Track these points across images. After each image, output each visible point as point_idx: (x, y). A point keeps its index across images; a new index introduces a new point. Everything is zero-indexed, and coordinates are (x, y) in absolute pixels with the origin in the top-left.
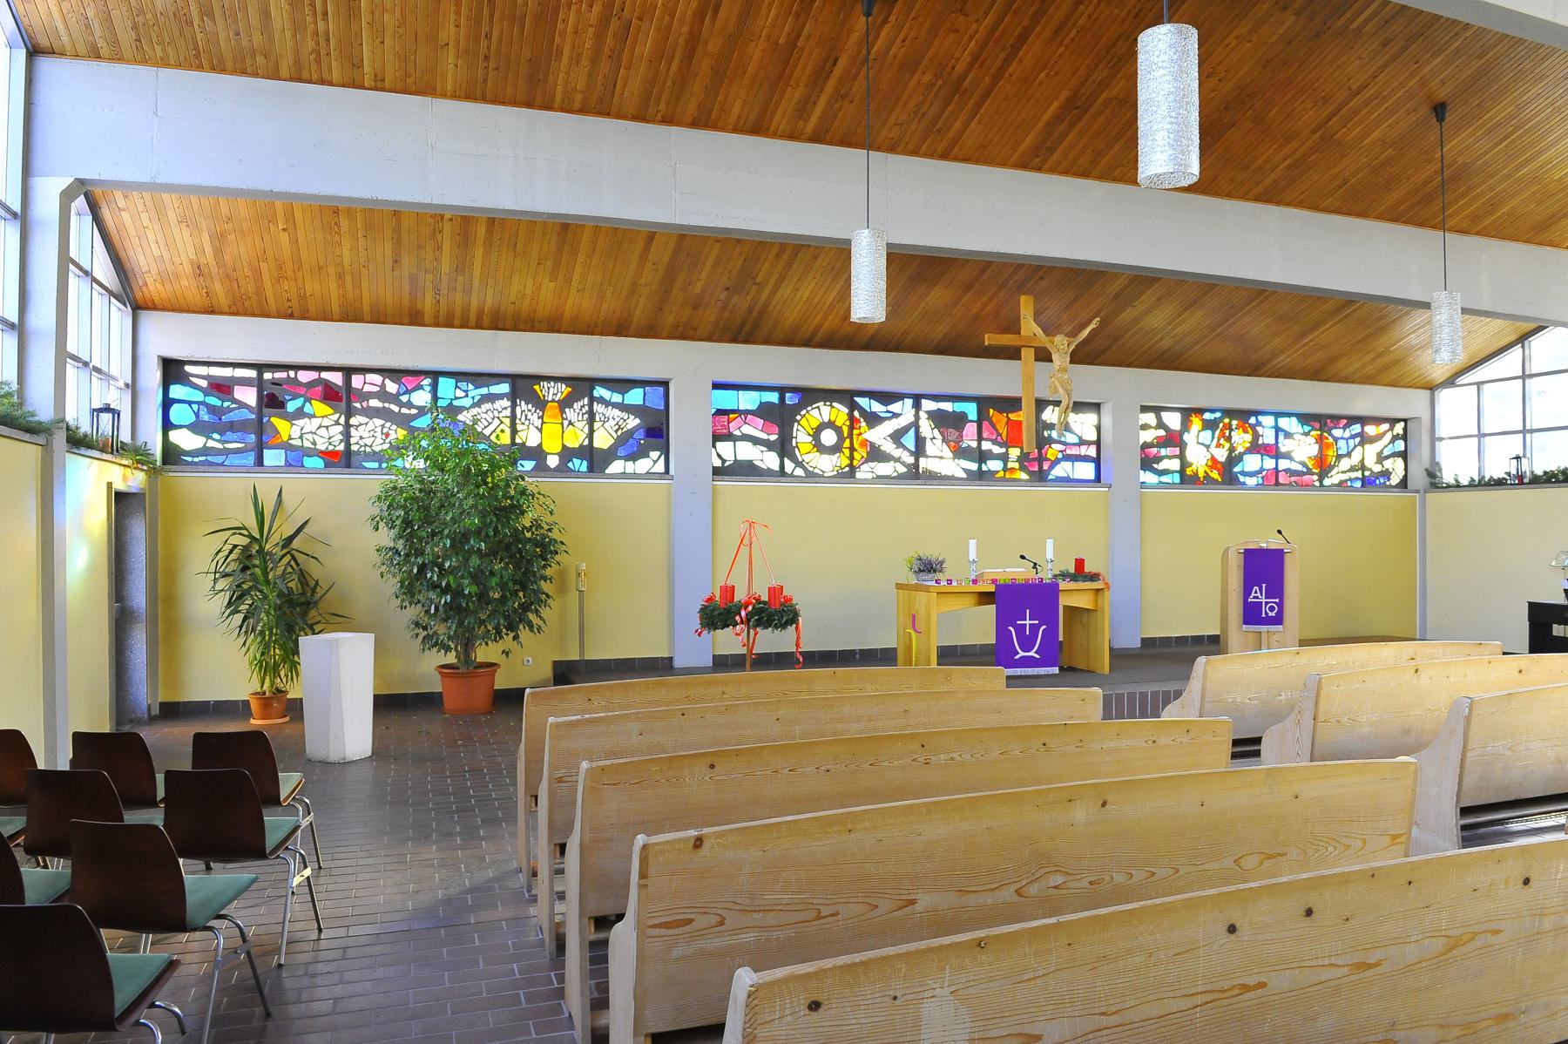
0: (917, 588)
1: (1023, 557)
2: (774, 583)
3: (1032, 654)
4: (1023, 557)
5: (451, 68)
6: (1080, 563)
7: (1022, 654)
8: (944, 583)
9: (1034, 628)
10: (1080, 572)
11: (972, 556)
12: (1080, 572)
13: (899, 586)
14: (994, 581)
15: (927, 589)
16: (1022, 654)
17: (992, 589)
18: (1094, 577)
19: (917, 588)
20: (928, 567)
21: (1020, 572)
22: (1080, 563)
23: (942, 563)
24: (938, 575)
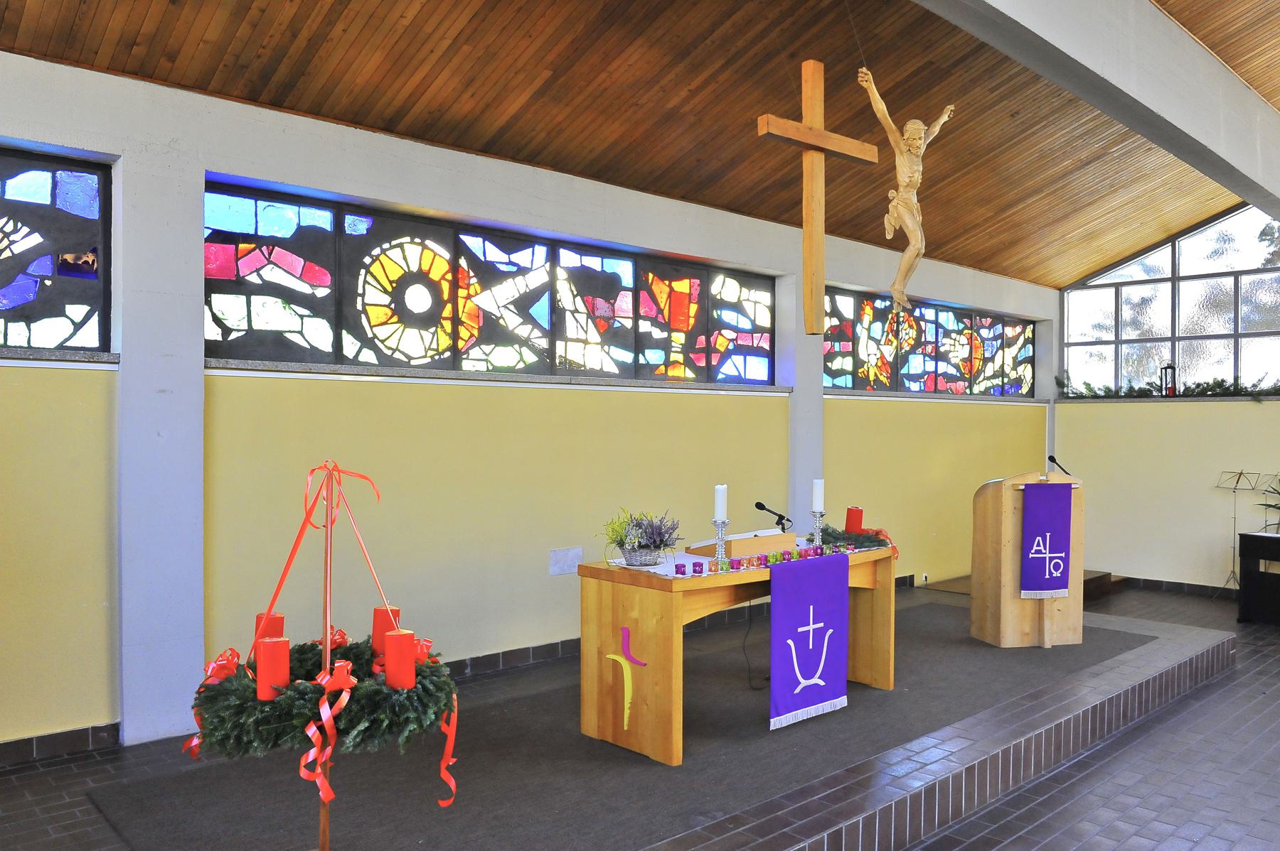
0: (633, 577)
1: (760, 506)
4: (760, 506)
6: (854, 516)
7: (804, 683)
9: (819, 634)
10: (857, 534)
13: (587, 572)
14: (763, 561)
15: (664, 585)
17: (763, 575)
18: (875, 539)
20: (656, 538)
22: (854, 516)
23: (674, 528)
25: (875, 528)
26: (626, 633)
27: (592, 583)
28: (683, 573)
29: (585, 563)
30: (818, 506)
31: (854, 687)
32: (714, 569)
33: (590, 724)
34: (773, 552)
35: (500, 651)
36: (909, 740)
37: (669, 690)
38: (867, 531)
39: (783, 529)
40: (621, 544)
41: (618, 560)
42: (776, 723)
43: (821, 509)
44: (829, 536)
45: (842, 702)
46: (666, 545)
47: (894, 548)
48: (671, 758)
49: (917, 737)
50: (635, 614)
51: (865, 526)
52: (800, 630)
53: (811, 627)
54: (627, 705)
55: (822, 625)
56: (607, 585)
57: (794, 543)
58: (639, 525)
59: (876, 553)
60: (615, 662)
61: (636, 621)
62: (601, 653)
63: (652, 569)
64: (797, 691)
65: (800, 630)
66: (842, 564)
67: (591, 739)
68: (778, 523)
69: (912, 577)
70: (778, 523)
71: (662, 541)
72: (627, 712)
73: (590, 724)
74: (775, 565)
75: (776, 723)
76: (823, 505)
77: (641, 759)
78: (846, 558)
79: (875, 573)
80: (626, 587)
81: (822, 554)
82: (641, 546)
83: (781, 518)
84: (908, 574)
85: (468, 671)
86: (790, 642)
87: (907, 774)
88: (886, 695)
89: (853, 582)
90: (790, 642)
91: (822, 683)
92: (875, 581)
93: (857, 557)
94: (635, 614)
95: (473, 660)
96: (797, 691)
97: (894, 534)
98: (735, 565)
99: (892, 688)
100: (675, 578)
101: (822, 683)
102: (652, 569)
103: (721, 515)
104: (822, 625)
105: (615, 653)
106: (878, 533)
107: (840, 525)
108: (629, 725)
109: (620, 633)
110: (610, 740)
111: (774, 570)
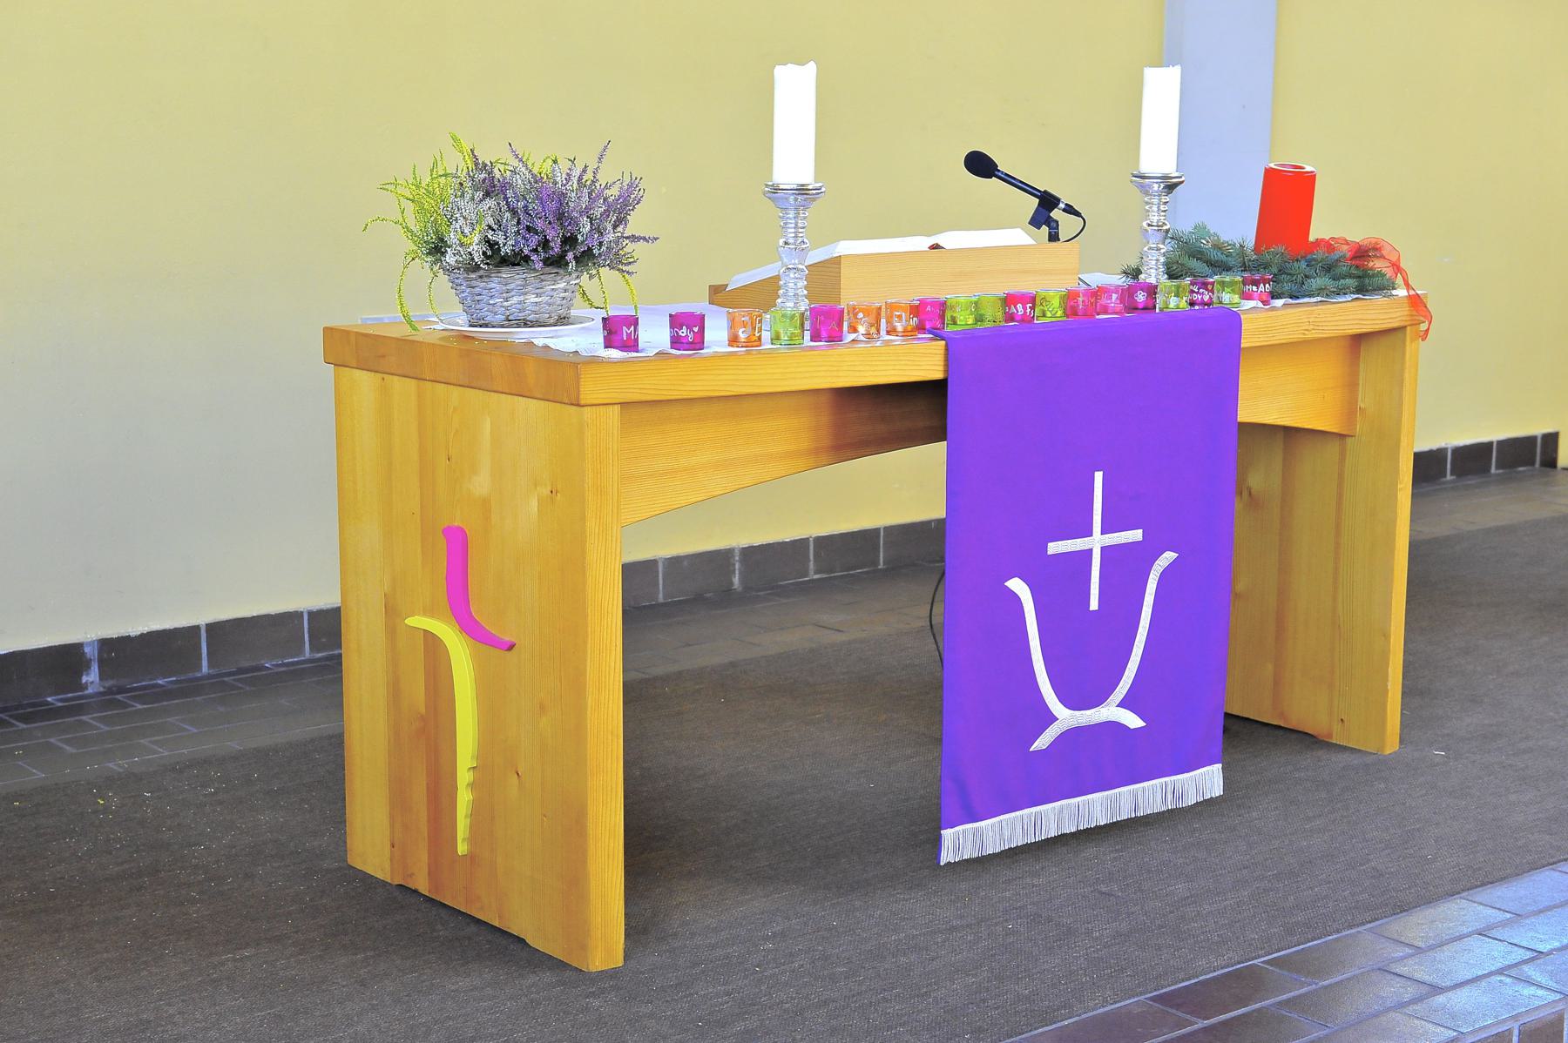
0: (475, 364)
1: (980, 165)
2: (1283, 158)
3: (1111, 711)
4: (980, 165)
5: (634, 675)
6: (1287, 194)
7: (1066, 717)
8: (654, 335)
9: (1125, 568)
10: (1288, 245)
11: (794, 162)
12: (1288, 245)
13: (351, 349)
14: (929, 317)
15: (559, 380)
16: (1066, 717)
17: (923, 362)
18: (1359, 270)
19: (475, 364)
20: (550, 235)
21: (989, 256)
22: (1287, 194)
23: (621, 209)
24: (603, 290)
25: (1357, 234)
26: (457, 541)
27: (364, 381)
28: (631, 345)
29: (340, 321)
30: (1158, 153)
31: (1242, 735)
32: (745, 343)
33: (371, 845)
34: (971, 302)
35: (202, 616)
36: (1403, 908)
37: (576, 732)
38: (1328, 245)
39: (1054, 237)
40: (438, 249)
41: (439, 309)
42: (958, 842)
43: (1169, 167)
44: (1195, 260)
45: (1208, 781)
46: (586, 258)
47: (1416, 302)
48: (583, 947)
49: (1428, 899)
50: (481, 484)
51: (1319, 230)
52: (1054, 548)
53: (1097, 541)
54: (464, 777)
55: (1136, 535)
56: (403, 388)
57: (1054, 275)
58: (491, 188)
59: (1349, 314)
60: (431, 641)
61: (485, 504)
62: (392, 612)
63: (540, 337)
64: (1042, 742)
65: (1054, 548)
66: (1218, 342)
67: (366, 878)
68: (1036, 222)
69: (1551, 440)
70: (1036, 222)
71: (570, 241)
72: (464, 798)
73: (371, 845)
74: (969, 337)
75: (958, 842)
76: (1162, 150)
77: (503, 947)
78: (1233, 321)
79: (1352, 385)
80: (456, 392)
81: (1150, 307)
82: (498, 258)
83: (1048, 201)
84: (1537, 429)
85: (92, 677)
86: (1017, 585)
87: (1402, 1005)
88: (1375, 766)
89: (1259, 402)
90: (1017, 585)
91: (1133, 721)
92: (1351, 410)
93: (1263, 321)
94: (481, 484)
95: (106, 644)
96: (1042, 742)
97: (1421, 264)
98: (826, 324)
99: (1392, 745)
100: (594, 361)
101: (1133, 721)
102: (540, 337)
103: (794, 162)
104: (1136, 535)
105: (430, 612)
106: (1362, 253)
107: (1238, 225)
108: (473, 839)
109: (442, 544)
110: (424, 889)
111: (957, 348)
